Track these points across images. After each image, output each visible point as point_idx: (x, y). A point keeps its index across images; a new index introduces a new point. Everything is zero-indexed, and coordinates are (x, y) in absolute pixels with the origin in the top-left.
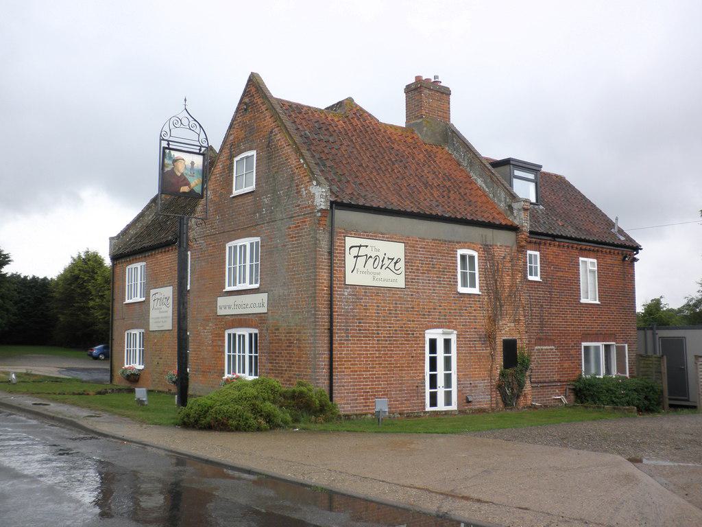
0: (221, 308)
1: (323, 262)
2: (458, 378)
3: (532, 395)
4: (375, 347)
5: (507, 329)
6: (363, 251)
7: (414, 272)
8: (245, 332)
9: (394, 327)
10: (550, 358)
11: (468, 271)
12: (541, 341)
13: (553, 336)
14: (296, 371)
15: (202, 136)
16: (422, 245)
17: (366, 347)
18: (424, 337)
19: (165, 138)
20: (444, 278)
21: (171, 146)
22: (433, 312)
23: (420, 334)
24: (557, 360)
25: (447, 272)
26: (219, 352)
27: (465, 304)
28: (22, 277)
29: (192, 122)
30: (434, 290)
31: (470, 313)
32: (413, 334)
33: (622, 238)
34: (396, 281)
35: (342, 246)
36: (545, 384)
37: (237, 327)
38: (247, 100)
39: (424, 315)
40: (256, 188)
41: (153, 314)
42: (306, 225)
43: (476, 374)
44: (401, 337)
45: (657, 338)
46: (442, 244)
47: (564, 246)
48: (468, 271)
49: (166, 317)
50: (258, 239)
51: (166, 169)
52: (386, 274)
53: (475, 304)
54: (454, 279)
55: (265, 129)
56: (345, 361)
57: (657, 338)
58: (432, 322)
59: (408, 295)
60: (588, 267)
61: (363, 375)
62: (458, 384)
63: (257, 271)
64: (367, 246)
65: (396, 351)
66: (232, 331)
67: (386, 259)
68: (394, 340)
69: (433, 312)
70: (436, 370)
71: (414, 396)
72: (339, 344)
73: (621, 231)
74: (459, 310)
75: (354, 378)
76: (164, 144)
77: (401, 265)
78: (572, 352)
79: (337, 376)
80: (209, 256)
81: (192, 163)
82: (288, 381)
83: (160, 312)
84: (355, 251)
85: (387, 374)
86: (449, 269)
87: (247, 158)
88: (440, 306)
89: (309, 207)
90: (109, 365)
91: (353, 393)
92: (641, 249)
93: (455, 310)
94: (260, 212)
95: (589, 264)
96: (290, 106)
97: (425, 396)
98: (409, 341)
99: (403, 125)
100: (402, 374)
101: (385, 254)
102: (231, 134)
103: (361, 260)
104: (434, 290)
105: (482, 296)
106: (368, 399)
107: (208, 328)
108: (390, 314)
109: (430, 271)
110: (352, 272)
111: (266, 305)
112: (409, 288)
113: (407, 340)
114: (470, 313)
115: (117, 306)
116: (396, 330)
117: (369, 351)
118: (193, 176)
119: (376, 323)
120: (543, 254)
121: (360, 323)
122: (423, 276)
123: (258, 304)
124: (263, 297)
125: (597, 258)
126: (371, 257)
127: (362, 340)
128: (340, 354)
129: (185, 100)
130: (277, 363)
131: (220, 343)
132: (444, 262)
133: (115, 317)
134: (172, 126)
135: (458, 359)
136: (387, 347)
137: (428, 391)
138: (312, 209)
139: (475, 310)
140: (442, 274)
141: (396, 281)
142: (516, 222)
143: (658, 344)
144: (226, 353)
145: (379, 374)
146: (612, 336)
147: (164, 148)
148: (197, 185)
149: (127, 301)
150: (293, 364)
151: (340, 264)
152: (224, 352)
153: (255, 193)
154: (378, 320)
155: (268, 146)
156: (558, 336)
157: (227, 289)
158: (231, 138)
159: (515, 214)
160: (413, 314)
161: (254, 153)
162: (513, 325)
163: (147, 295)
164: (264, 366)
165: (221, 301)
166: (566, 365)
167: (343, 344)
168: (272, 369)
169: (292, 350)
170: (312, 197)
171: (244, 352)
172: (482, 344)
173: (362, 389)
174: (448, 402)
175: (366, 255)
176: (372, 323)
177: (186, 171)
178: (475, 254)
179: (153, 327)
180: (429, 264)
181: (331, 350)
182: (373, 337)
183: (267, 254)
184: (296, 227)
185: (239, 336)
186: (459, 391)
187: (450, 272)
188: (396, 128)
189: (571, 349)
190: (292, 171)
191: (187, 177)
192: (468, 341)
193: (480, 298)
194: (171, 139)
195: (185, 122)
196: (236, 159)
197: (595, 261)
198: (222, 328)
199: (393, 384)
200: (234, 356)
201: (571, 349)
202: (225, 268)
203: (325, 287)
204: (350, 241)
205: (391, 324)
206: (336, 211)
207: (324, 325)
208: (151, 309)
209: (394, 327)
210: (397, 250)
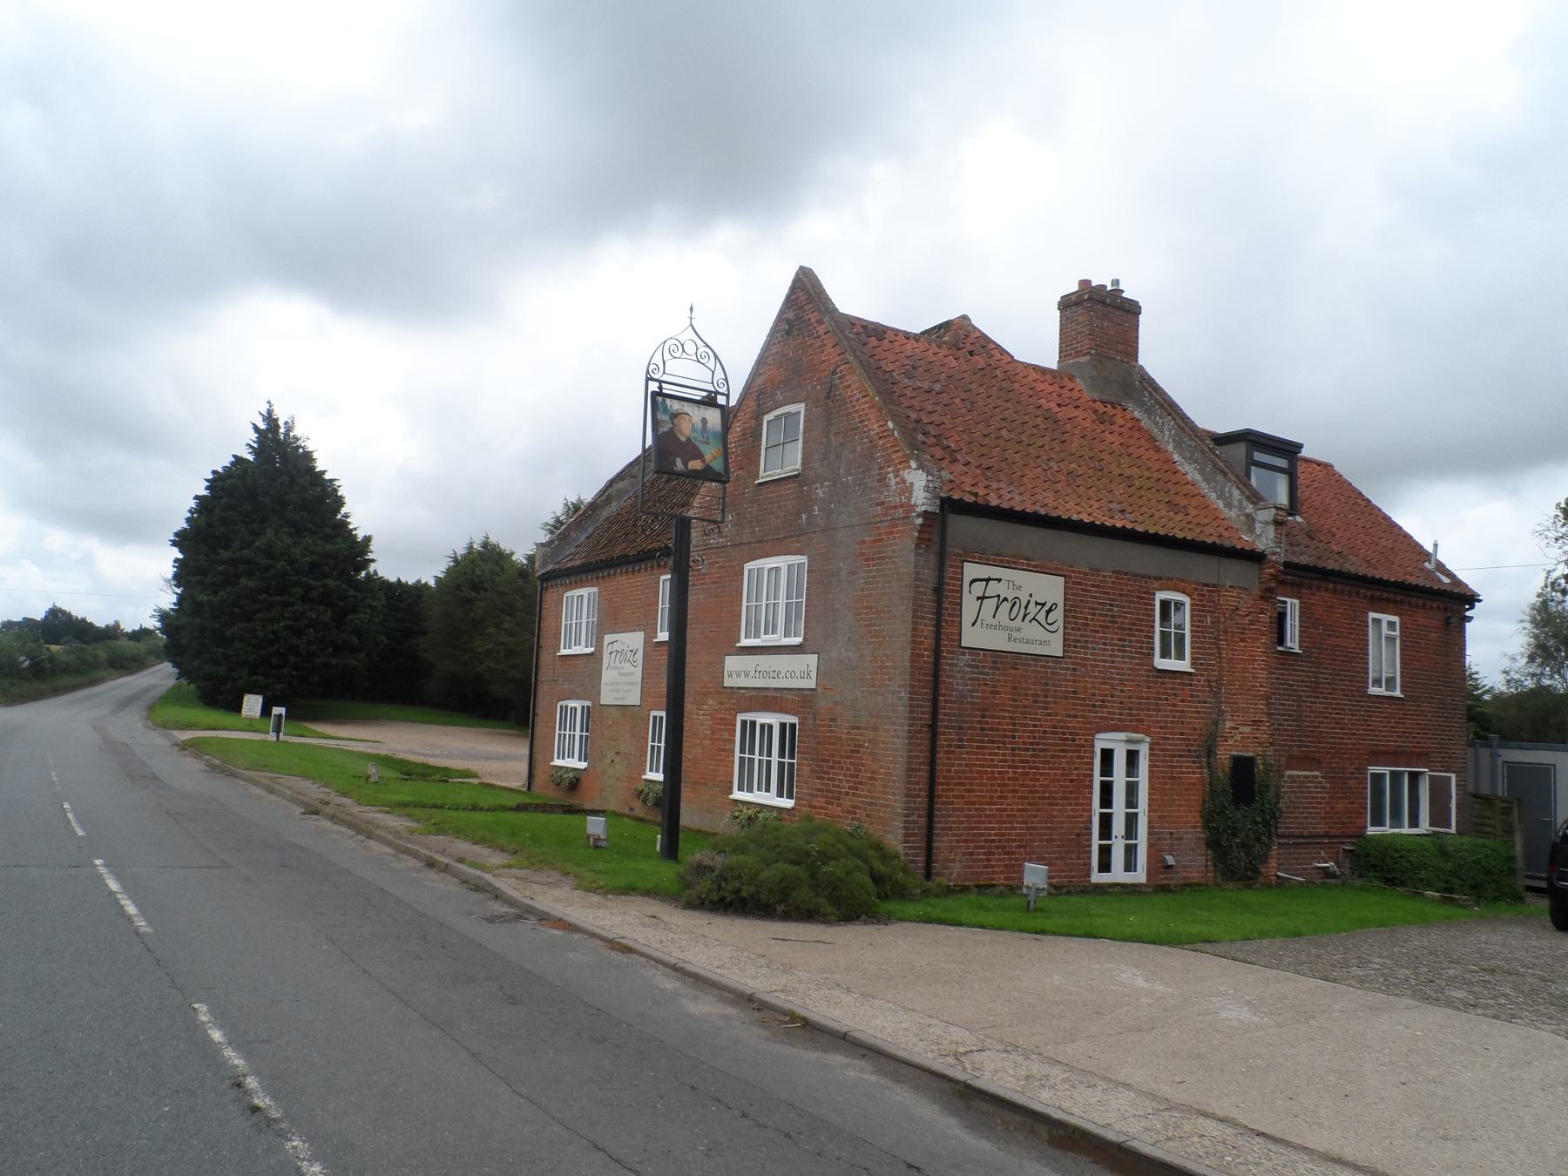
0: (730, 676)
1: (925, 606)
2: (1149, 822)
3: (1278, 859)
4: (1006, 761)
5: (1239, 737)
6: (993, 589)
7: (1079, 630)
8: (773, 719)
9: (1041, 726)
10: (1311, 793)
11: (1173, 630)
12: (1294, 761)
13: (1319, 752)
14: (866, 797)
15: (719, 375)
16: (1095, 581)
17: (993, 760)
18: (1093, 746)
19: (654, 376)
20: (1131, 641)
21: (664, 391)
22: (1109, 701)
23: (1086, 740)
24: (1324, 798)
25: (1137, 630)
26: (724, 750)
27: (1165, 688)
28: (339, 494)
29: (703, 349)
30: (1113, 662)
31: (1174, 705)
32: (1073, 740)
33: (1446, 580)
34: (1047, 643)
35: (958, 579)
36: (1301, 840)
37: (759, 711)
38: (790, 315)
39: (1093, 706)
40: (803, 469)
41: (607, 675)
42: (894, 539)
43: (1181, 817)
44: (1053, 745)
45: (1500, 765)
46: (1129, 579)
47: (1343, 592)
48: (1173, 630)
49: (631, 684)
50: (803, 559)
51: (662, 430)
52: (1032, 631)
53: (1182, 690)
54: (1148, 643)
55: (823, 367)
56: (955, 784)
57: (1500, 765)
58: (1107, 719)
59: (1067, 669)
60: (1384, 629)
61: (985, 810)
62: (1150, 834)
63: (798, 617)
64: (999, 580)
65: (1044, 768)
66: (749, 717)
67: (1032, 604)
68: (1041, 750)
69: (1109, 701)
70: (1127, 814)
71: (1073, 852)
72: (946, 752)
73: (1441, 567)
74: (1155, 699)
75: (968, 816)
76: (653, 386)
77: (1058, 615)
78: (1351, 783)
79: (940, 809)
80: (713, 583)
81: (704, 421)
82: (849, 812)
83: (620, 674)
84: (979, 588)
85: (1026, 810)
86: (1141, 625)
87: (787, 415)
88: (1122, 691)
89: (901, 506)
90: (528, 745)
91: (966, 841)
92: (1480, 601)
93: (1148, 698)
94: (810, 512)
95: (1384, 626)
96: (863, 327)
97: (1090, 852)
98: (1066, 751)
99: (1054, 366)
100: (1054, 810)
101: (1031, 596)
102: (760, 374)
103: (990, 605)
104: (1113, 662)
105: (1196, 675)
106: (993, 854)
107: (705, 707)
108: (1036, 701)
109: (1108, 627)
110: (973, 625)
111: (814, 675)
112: (1070, 657)
113: (1062, 751)
114: (1174, 705)
115: (545, 658)
116: (1045, 732)
117: (996, 766)
118: (708, 444)
119: (1011, 718)
120: (1305, 603)
121: (983, 716)
122: (1094, 637)
123: (800, 672)
124: (812, 660)
125: (1399, 614)
126: (1005, 599)
127: (985, 748)
128: (948, 771)
129: (691, 309)
130: (829, 779)
131: (726, 735)
132: (1131, 613)
133: (542, 678)
134: (667, 356)
135: (1152, 787)
136: (1028, 762)
137: (1096, 842)
138: (907, 512)
139: (1182, 701)
140: (1128, 635)
141: (1047, 643)
142: (1260, 546)
143: (1501, 771)
144: (737, 754)
145: (1012, 810)
146: (1421, 757)
148: (715, 458)
149: (564, 652)
150: (861, 783)
151: (954, 610)
152: (733, 752)
153: (800, 478)
154: (1014, 712)
155: (828, 397)
156: (1327, 753)
157: (745, 642)
158: (760, 380)
159: (1258, 531)
160: (1076, 704)
161: (800, 408)
162: (1247, 729)
164: (806, 782)
165: (732, 663)
166: (1339, 807)
167: (953, 753)
168: (822, 790)
169: (861, 759)
170: (908, 489)
171: (769, 754)
172: (1194, 762)
173: (983, 835)
174: (1130, 866)
175: (998, 596)
176: (1004, 718)
177: (696, 435)
178: (1186, 600)
179: (607, 698)
180: (1106, 615)
181: (932, 763)
182: (1004, 743)
183: (821, 581)
184: (875, 541)
185: (762, 726)
186: (1150, 846)
187: (1142, 631)
188: (1044, 371)
189: (1350, 778)
190: (871, 442)
191: (697, 444)
192: (1170, 756)
193: (1193, 680)
194: (665, 378)
195: (690, 348)
196: (767, 418)
197: (1396, 619)
198: (731, 709)
199: (1036, 828)
200: (751, 761)
201: (1350, 778)
202: (741, 605)
203: (926, 650)
204: (971, 570)
205: (1035, 720)
206: (949, 515)
207: (921, 719)
208: (604, 667)
209: (1041, 726)
210: (1051, 588)
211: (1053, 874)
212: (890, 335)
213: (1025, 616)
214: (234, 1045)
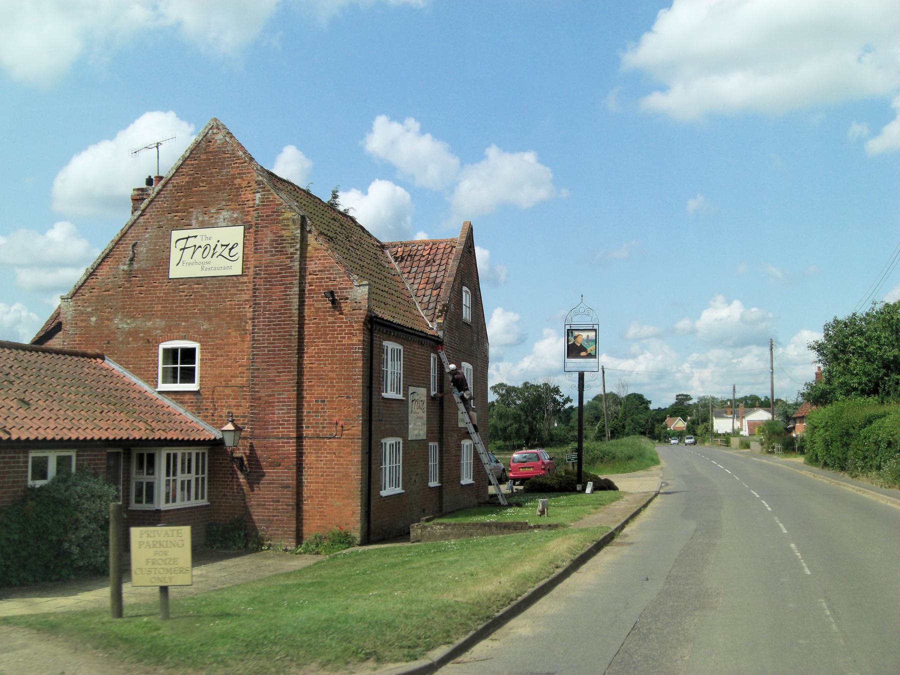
6: (191, 242)
11: (179, 366)
48: (179, 366)
51: (570, 343)
67: (219, 244)
76: (568, 327)
77: (239, 250)
81: (588, 336)
84: (181, 244)
147: (568, 330)
163: (406, 394)
175: (195, 246)
211: (24, 474)
212: (169, 237)
213: (213, 254)
214: (550, 407)
